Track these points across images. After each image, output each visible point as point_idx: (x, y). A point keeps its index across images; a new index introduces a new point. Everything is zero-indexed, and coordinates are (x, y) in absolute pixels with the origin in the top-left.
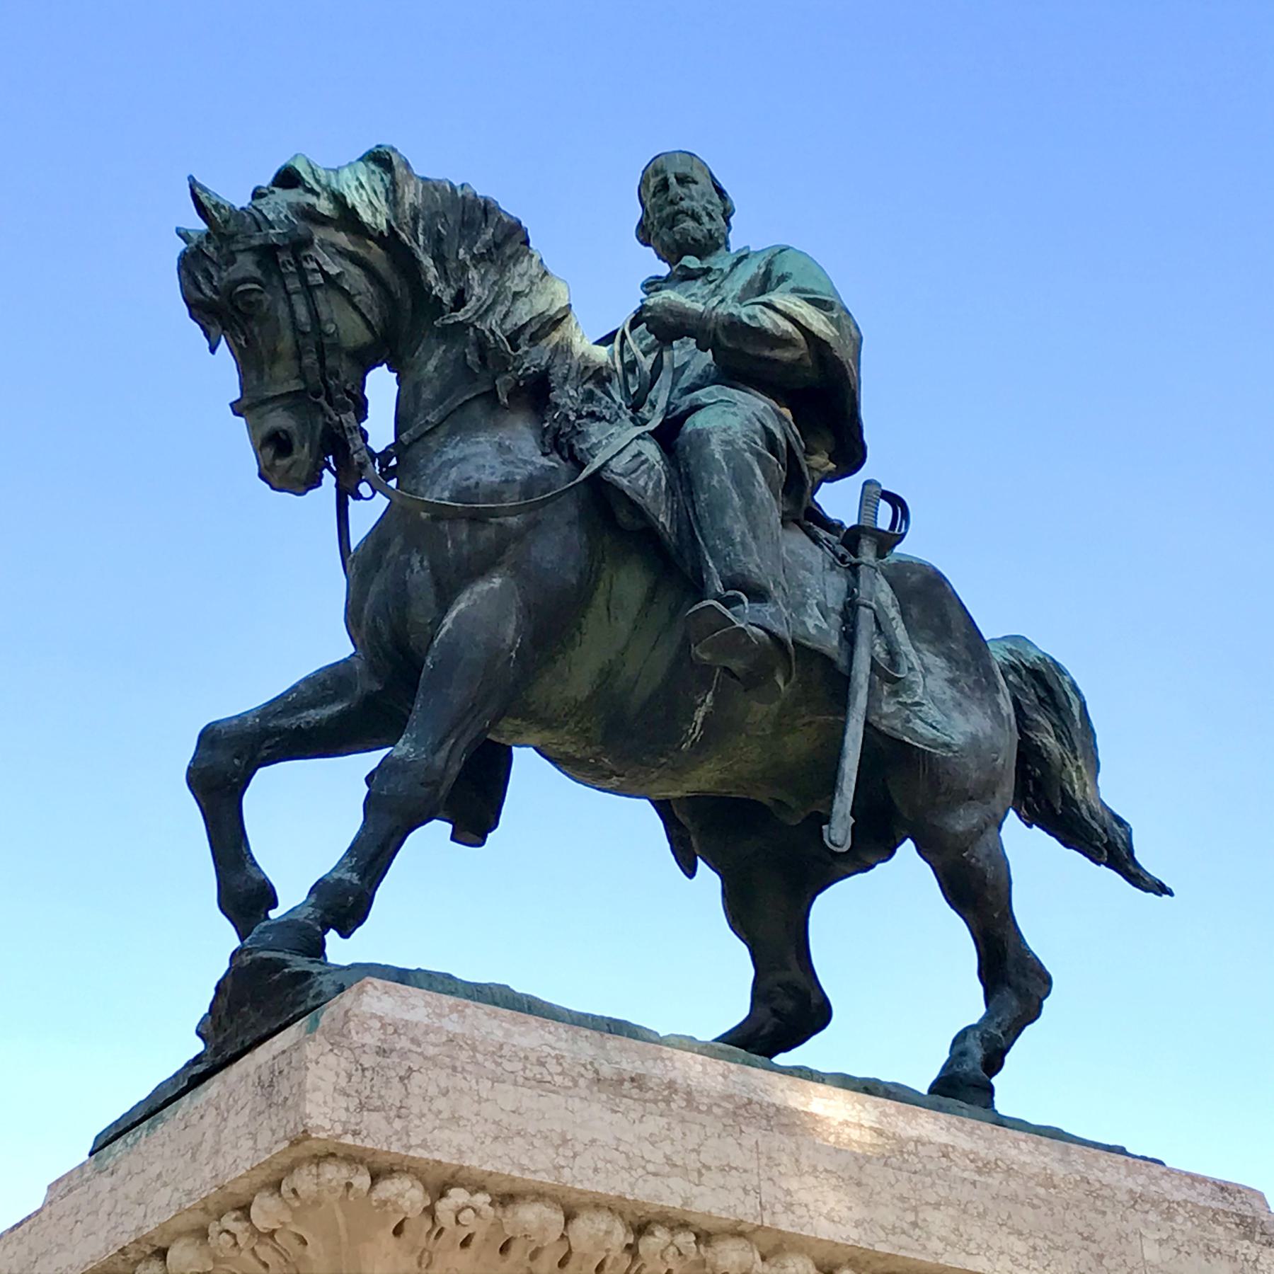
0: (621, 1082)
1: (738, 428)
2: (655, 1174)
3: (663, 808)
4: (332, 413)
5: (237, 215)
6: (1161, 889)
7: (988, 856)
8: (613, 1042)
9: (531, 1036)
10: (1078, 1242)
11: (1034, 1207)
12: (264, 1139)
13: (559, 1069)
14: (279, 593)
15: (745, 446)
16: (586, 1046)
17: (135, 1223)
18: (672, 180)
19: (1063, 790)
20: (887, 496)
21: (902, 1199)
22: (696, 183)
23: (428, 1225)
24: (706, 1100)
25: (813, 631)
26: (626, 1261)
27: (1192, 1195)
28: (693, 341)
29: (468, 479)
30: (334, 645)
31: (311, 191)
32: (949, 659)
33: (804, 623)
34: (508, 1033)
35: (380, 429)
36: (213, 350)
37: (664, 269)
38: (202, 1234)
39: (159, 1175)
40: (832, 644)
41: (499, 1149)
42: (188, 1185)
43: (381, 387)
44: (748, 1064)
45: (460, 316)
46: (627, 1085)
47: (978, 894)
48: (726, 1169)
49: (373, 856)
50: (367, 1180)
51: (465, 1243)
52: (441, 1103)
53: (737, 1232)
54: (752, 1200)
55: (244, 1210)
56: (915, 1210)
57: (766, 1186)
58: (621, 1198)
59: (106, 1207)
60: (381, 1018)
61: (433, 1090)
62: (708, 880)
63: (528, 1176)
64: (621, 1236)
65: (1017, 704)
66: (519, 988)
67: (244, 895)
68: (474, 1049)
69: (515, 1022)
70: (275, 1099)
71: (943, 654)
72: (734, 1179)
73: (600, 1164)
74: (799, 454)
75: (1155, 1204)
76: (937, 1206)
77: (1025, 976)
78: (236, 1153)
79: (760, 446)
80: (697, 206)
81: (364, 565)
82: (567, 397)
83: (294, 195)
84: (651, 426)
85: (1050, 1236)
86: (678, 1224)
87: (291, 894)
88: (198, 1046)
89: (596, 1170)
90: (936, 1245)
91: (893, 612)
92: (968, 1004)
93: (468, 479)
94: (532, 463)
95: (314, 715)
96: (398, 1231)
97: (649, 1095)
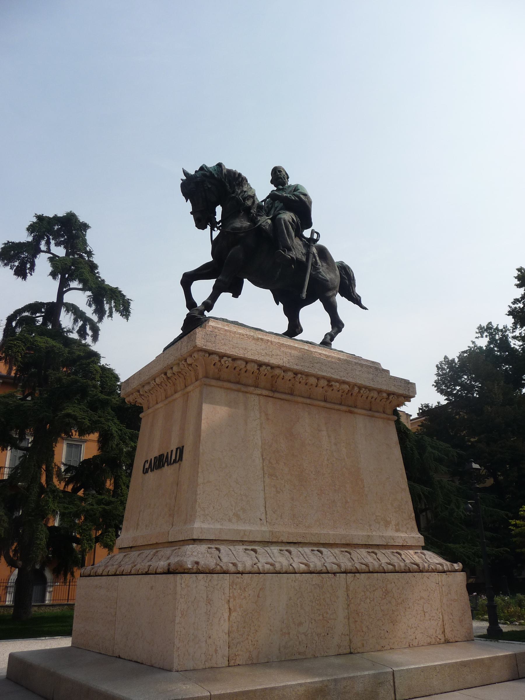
6: (366, 309)
8: (258, 332)
12: (189, 347)
14: (198, 247)
20: (316, 232)
27: (367, 363)
30: (210, 259)
35: (218, 217)
37: (275, 189)
38: (178, 364)
41: (233, 350)
42: (176, 355)
43: (219, 209)
45: (233, 195)
47: (331, 309)
49: (214, 297)
50: (208, 355)
51: (227, 367)
52: (222, 341)
55: (186, 360)
61: (221, 339)
62: (281, 305)
64: (256, 367)
65: (340, 274)
67: (190, 303)
69: (239, 328)
72: (278, 357)
76: (317, 363)
79: (291, 221)
81: (215, 243)
82: (254, 211)
83: (202, 172)
84: (270, 217)
88: (182, 332)
91: (316, 255)
92: (328, 328)
95: (205, 271)
96: (214, 365)
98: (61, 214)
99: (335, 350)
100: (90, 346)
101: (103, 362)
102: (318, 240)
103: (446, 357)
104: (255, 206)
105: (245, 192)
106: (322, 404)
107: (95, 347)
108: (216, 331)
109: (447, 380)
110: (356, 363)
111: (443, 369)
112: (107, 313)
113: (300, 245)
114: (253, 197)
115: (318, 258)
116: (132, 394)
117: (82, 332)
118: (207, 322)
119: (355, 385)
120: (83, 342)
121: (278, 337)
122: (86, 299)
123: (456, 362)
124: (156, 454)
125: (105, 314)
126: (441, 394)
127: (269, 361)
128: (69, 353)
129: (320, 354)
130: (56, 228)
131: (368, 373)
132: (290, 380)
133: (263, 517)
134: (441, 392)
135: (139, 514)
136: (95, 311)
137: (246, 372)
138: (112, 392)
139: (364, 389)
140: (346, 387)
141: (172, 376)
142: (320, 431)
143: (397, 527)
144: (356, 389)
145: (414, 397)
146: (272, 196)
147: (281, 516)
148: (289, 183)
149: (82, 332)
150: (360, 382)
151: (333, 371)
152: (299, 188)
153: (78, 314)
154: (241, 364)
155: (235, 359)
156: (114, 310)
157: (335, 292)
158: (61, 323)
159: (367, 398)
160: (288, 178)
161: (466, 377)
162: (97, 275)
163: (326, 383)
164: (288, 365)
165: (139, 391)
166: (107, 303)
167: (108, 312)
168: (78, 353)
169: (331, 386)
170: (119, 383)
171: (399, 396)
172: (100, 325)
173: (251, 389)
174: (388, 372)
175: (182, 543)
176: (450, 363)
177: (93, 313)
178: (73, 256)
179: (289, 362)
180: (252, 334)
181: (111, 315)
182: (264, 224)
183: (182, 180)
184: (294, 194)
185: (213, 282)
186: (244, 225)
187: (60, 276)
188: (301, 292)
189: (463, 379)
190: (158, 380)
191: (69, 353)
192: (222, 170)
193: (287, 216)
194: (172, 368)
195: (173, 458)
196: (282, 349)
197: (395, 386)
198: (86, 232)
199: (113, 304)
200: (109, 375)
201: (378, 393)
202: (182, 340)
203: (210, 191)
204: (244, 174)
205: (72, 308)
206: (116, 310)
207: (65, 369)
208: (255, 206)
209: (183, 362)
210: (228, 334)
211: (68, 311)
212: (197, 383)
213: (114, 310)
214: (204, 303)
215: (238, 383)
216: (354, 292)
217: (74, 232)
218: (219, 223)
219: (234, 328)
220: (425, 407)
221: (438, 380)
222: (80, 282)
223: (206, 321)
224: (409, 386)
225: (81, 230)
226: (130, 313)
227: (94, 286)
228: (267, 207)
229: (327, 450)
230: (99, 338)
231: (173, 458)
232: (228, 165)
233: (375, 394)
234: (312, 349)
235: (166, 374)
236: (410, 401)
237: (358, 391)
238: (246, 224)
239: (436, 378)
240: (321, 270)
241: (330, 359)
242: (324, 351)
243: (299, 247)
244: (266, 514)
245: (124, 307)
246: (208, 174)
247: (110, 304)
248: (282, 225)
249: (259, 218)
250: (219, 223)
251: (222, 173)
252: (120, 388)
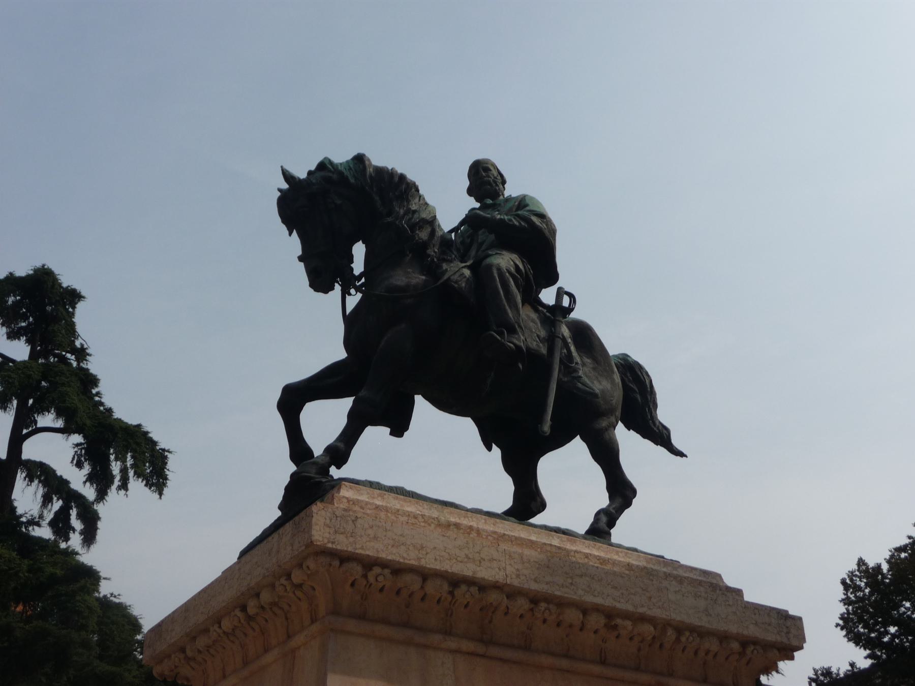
5: (301, 181)
6: (681, 454)
8: (447, 510)
9: (411, 507)
14: (317, 329)
16: (434, 512)
21: (566, 573)
23: (365, 583)
26: (449, 598)
30: (341, 354)
31: (330, 171)
34: (402, 506)
35: (358, 266)
36: (290, 235)
37: (478, 205)
38: (273, 586)
41: (394, 550)
43: (359, 251)
45: (390, 219)
47: (606, 456)
48: (492, 560)
49: (350, 436)
51: (381, 590)
52: (370, 532)
56: (572, 578)
57: (508, 567)
58: (446, 572)
60: (347, 498)
61: (366, 526)
62: (496, 451)
63: (406, 561)
64: (446, 587)
66: (408, 488)
69: (405, 501)
76: (581, 576)
79: (513, 270)
81: (350, 320)
82: (433, 251)
87: (318, 449)
88: (279, 513)
89: (436, 559)
90: (580, 592)
91: (569, 340)
92: (602, 500)
96: (353, 585)
98: (22, 270)
99: (619, 546)
100: (77, 554)
101: (105, 589)
102: (572, 310)
103: (861, 562)
104: (436, 241)
105: (414, 212)
106: (597, 669)
107: (88, 557)
108: (357, 508)
109: (868, 612)
110: (667, 576)
111: (857, 588)
112: (117, 482)
113: (533, 321)
114: (432, 222)
115: (573, 348)
116: (169, 656)
117: (61, 525)
118: (336, 489)
119: (667, 624)
120: (63, 545)
121: (493, 520)
122: (71, 452)
123: (885, 571)
125: (112, 482)
126: (857, 644)
127: (474, 573)
128: (29, 571)
129: (587, 556)
130: (11, 300)
132: (521, 616)
134: (856, 639)
136: (90, 478)
137: (423, 599)
138: (124, 656)
139: (687, 633)
140: (648, 630)
141: (257, 614)
144: (671, 634)
145: (801, 648)
146: (471, 220)
148: (507, 193)
149: (61, 525)
150: (677, 616)
152: (528, 201)
153: (53, 484)
154: (412, 582)
155: (398, 570)
156: (131, 473)
157: (613, 419)
158: (16, 504)
159: (696, 653)
160: (504, 182)
161: (908, 605)
162: (97, 399)
163: (602, 621)
164: (516, 583)
165: (183, 650)
166: (116, 459)
167: (118, 478)
168: (49, 570)
169: (615, 627)
170: (139, 637)
171: (767, 646)
172: (100, 508)
173: (436, 638)
174: (739, 592)
176: (871, 574)
177: (85, 483)
178: (46, 358)
179: (518, 576)
180: (435, 514)
181: (124, 486)
182: (456, 277)
183: (280, 190)
184: (518, 216)
185: (347, 403)
186: (414, 281)
187: (15, 402)
188: (540, 419)
189: (903, 609)
190: (226, 624)
191: (29, 571)
192: (365, 168)
193: (505, 261)
194: (258, 595)
196: (504, 546)
197: (756, 624)
198: (74, 308)
199: (129, 461)
200: (117, 617)
201: (721, 642)
202: (281, 531)
203: (341, 213)
204: (411, 176)
205: (41, 473)
206: (135, 473)
207: (20, 608)
208: (436, 241)
209: (283, 581)
210: (383, 515)
211: (30, 478)
212: (315, 628)
213: (131, 473)
214: (329, 450)
215: (406, 625)
216: (653, 418)
217: (49, 308)
218: (359, 278)
219: (394, 502)
220: (823, 674)
221: (848, 613)
222: (59, 415)
223: (333, 487)
224: (789, 623)
225: (64, 305)
226: (166, 479)
227: (88, 422)
228: (462, 243)
230: (97, 537)
232: (378, 159)
233: (712, 645)
234: (569, 546)
235: (244, 608)
236: (792, 658)
237: (674, 637)
238: (418, 278)
239: (842, 609)
240: (581, 373)
241: (608, 567)
242: (596, 550)
243: (531, 324)
245: (153, 466)
246: (335, 176)
247: (124, 461)
248: (499, 293)
249: (445, 266)
250: (359, 278)
251: (365, 175)
252: (142, 648)
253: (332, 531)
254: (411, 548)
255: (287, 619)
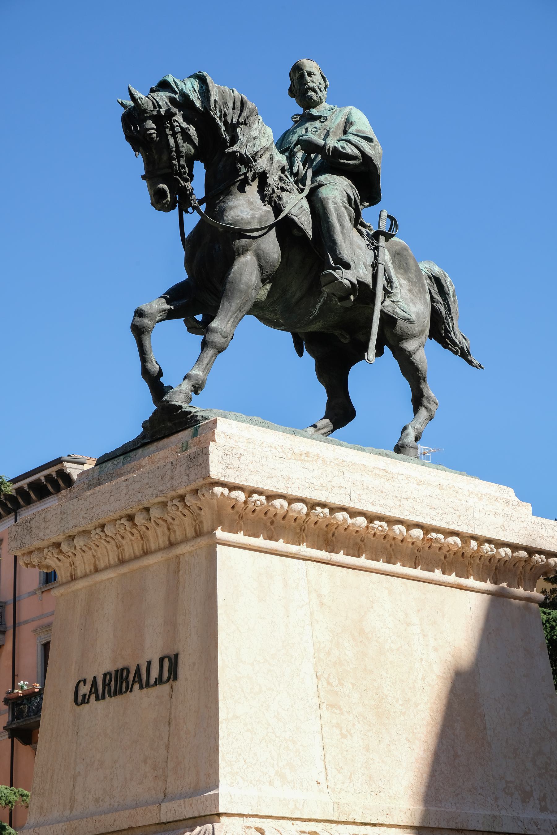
0: (301, 455)
1: (338, 197)
2: (317, 490)
3: (293, 334)
4: (182, 182)
7: (420, 359)
10: (452, 511)
11: (438, 499)
13: (281, 450)
15: (341, 205)
17: (138, 499)
18: (306, 74)
19: (445, 326)
21: (396, 497)
22: (314, 75)
24: (329, 461)
25: (362, 275)
28: (537, 555)
29: (238, 216)
30: (184, 276)
32: (409, 281)
33: (358, 271)
39: (147, 484)
40: (368, 280)
44: (340, 445)
45: (234, 148)
46: (303, 456)
52: (251, 466)
53: (343, 509)
54: (348, 498)
57: (353, 493)
59: (124, 492)
61: (248, 462)
68: (254, 444)
70: (196, 463)
71: (407, 279)
73: (300, 487)
74: (359, 203)
75: (476, 495)
76: (407, 499)
77: (430, 403)
78: (180, 480)
80: (314, 85)
85: (443, 509)
86: (323, 505)
89: (299, 488)
93: (238, 216)
94: (261, 209)
97: (311, 459)
124: (108, 666)
131: (496, 514)
133: (322, 780)
135: (75, 781)
142: (408, 624)
143: (543, 804)
147: (350, 778)
151: (434, 513)
175: (190, 822)
195: (154, 674)
229: (421, 659)
231: (154, 674)
244: (327, 774)
253: (224, 467)
254: (281, 479)
255: (169, 529)
